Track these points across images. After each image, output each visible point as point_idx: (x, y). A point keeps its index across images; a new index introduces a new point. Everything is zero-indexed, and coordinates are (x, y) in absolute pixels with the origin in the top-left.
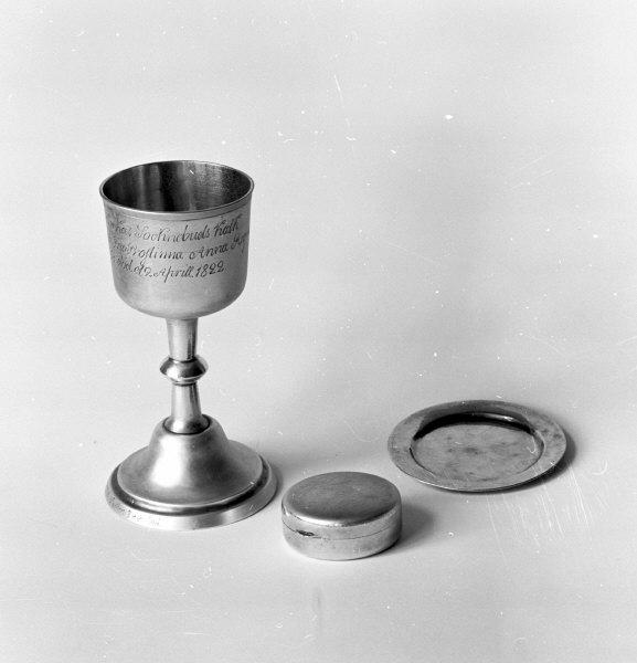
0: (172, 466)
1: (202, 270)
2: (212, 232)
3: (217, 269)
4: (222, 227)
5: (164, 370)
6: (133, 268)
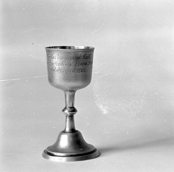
0: (65, 142)
1: (79, 70)
2: (82, 57)
3: (83, 71)
4: (86, 56)
5: (63, 111)
6: (56, 70)
